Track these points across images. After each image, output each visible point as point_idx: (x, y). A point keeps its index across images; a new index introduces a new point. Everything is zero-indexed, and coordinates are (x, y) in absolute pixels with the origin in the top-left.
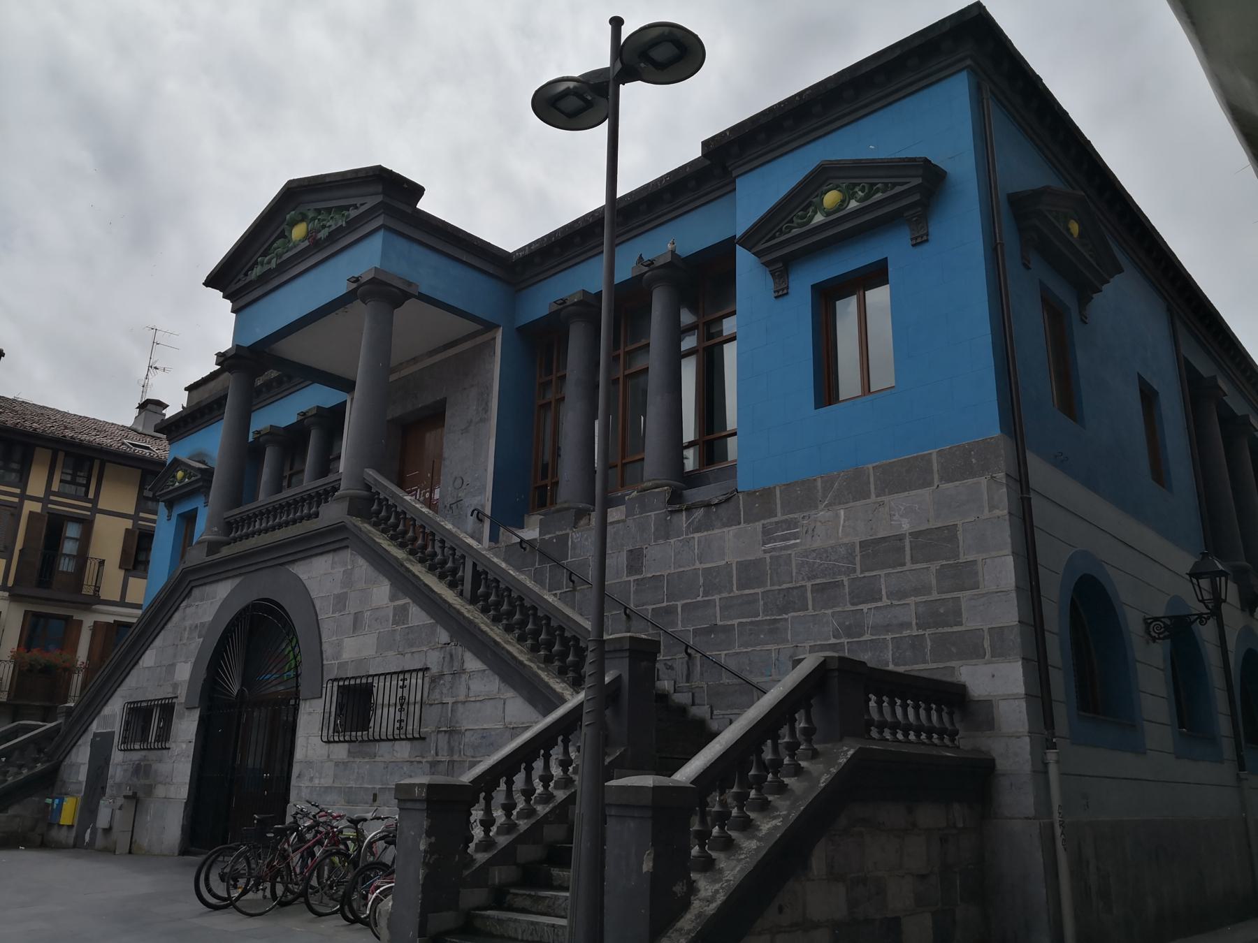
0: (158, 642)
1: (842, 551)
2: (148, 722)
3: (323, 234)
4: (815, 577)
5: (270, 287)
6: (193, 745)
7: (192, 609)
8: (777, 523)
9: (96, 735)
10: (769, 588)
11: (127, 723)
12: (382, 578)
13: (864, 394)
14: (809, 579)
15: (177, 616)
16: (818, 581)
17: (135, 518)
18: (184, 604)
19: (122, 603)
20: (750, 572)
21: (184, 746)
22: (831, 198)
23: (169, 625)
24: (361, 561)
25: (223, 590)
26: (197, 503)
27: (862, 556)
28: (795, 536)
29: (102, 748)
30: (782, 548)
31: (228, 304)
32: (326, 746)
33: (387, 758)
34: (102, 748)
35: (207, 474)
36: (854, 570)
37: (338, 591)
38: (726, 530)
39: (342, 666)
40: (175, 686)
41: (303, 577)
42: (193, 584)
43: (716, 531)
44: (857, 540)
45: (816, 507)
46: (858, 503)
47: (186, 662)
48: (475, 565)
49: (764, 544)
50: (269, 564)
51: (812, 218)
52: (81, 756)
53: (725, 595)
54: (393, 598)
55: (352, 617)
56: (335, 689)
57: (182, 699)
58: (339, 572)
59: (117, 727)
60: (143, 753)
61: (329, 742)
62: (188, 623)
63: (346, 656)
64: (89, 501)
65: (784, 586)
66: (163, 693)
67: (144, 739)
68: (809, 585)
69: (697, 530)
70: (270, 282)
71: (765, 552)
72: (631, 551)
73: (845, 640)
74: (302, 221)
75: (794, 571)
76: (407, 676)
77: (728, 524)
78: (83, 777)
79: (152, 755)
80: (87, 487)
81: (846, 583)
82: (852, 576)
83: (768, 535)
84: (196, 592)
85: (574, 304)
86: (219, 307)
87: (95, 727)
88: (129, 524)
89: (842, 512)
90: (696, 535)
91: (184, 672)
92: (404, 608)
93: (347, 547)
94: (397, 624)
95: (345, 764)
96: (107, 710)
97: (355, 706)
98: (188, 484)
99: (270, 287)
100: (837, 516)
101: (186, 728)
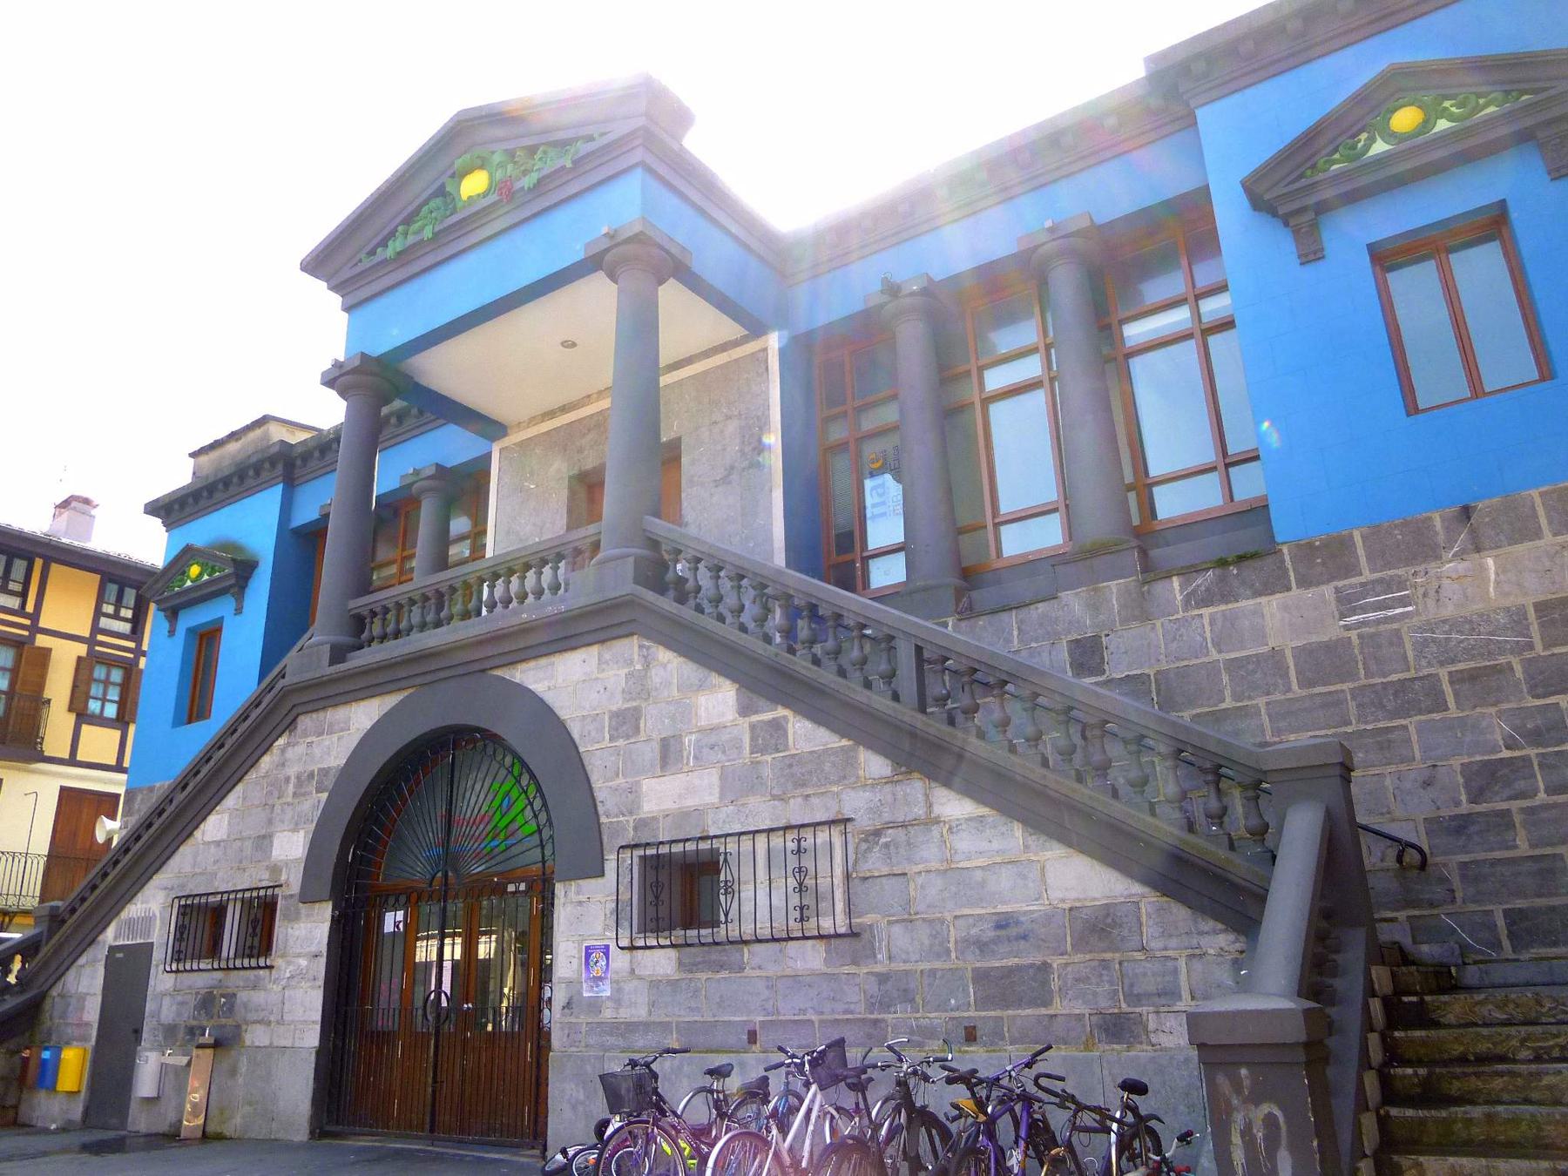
0: (231, 801)
1: (1502, 619)
2: (229, 929)
3: (528, 181)
4: (1453, 662)
5: (415, 268)
6: (323, 960)
7: (300, 749)
8: (1363, 585)
9: (112, 949)
10: (1364, 682)
11: (181, 930)
12: (715, 679)
13: (1542, 379)
14: (1442, 664)
15: (266, 762)
16: (1461, 666)
17: (91, 641)
18: (281, 741)
19: (72, 761)
20: (1324, 661)
21: (303, 962)
22: (1405, 119)
23: (252, 775)
24: (664, 655)
25: (363, 716)
26: (222, 608)
27: (1542, 625)
28: (1403, 602)
29: (128, 971)
30: (1378, 622)
31: (336, 300)
32: (627, 955)
33: (772, 970)
34: (128, 971)
35: (244, 569)
36: (1531, 646)
37: (618, 704)
38: (1263, 600)
39: (641, 825)
40: (275, 869)
41: (538, 687)
42: (300, 709)
43: (1243, 604)
44: (1529, 602)
45: (1438, 557)
46: (1520, 548)
47: (295, 830)
48: (919, 649)
49: (1342, 616)
50: (348, 687)
51: (1367, 147)
52: (86, 983)
53: (1278, 696)
54: (744, 710)
55: (656, 746)
56: (636, 860)
57: (295, 886)
58: (616, 677)
59: (160, 936)
60: (219, 975)
61: (632, 948)
62: (292, 771)
63: (649, 807)
64: (26, 616)
65: (1394, 677)
66: (253, 877)
67: (214, 950)
68: (1443, 673)
69: (1206, 602)
70: (413, 263)
71: (1347, 628)
72: (1077, 641)
73: (1532, 752)
74: (482, 167)
75: (1410, 654)
76: (803, 833)
77: (1267, 589)
78: (92, 1012)
79: (236, 978)
80: (24, 595)
81: (1518, 668)
82: (1528, 655)
83: (1347, 604)
84: (305, 722)
85: (912, 294)
86: (324, 301)
87: (110, 936)
88: (82, 650)
89: (1490, 562)
90: (1206, 612)
91: (291, 847)
92: (778, 726)
93: (632, 634)
94: (763, 751)
95: (673, 984)
96: (134, 910)
97: (682, 891)
98: (207, 583)
99: (415, 268)
100: (1483, 569)
101: (307, 935)
